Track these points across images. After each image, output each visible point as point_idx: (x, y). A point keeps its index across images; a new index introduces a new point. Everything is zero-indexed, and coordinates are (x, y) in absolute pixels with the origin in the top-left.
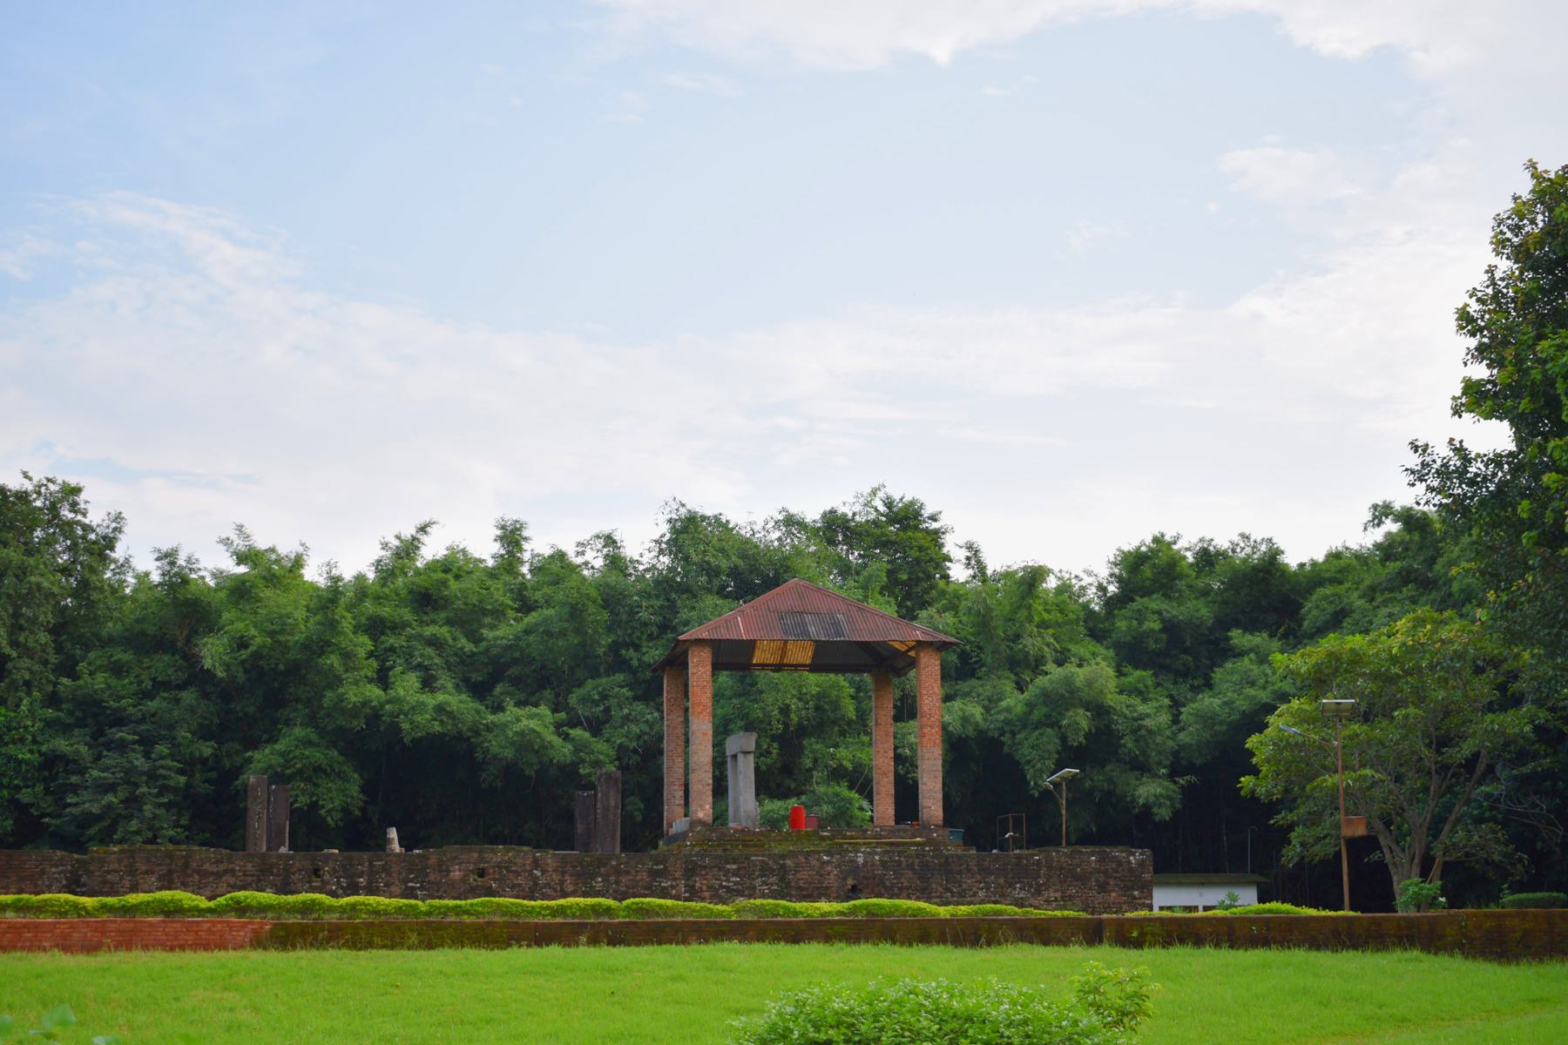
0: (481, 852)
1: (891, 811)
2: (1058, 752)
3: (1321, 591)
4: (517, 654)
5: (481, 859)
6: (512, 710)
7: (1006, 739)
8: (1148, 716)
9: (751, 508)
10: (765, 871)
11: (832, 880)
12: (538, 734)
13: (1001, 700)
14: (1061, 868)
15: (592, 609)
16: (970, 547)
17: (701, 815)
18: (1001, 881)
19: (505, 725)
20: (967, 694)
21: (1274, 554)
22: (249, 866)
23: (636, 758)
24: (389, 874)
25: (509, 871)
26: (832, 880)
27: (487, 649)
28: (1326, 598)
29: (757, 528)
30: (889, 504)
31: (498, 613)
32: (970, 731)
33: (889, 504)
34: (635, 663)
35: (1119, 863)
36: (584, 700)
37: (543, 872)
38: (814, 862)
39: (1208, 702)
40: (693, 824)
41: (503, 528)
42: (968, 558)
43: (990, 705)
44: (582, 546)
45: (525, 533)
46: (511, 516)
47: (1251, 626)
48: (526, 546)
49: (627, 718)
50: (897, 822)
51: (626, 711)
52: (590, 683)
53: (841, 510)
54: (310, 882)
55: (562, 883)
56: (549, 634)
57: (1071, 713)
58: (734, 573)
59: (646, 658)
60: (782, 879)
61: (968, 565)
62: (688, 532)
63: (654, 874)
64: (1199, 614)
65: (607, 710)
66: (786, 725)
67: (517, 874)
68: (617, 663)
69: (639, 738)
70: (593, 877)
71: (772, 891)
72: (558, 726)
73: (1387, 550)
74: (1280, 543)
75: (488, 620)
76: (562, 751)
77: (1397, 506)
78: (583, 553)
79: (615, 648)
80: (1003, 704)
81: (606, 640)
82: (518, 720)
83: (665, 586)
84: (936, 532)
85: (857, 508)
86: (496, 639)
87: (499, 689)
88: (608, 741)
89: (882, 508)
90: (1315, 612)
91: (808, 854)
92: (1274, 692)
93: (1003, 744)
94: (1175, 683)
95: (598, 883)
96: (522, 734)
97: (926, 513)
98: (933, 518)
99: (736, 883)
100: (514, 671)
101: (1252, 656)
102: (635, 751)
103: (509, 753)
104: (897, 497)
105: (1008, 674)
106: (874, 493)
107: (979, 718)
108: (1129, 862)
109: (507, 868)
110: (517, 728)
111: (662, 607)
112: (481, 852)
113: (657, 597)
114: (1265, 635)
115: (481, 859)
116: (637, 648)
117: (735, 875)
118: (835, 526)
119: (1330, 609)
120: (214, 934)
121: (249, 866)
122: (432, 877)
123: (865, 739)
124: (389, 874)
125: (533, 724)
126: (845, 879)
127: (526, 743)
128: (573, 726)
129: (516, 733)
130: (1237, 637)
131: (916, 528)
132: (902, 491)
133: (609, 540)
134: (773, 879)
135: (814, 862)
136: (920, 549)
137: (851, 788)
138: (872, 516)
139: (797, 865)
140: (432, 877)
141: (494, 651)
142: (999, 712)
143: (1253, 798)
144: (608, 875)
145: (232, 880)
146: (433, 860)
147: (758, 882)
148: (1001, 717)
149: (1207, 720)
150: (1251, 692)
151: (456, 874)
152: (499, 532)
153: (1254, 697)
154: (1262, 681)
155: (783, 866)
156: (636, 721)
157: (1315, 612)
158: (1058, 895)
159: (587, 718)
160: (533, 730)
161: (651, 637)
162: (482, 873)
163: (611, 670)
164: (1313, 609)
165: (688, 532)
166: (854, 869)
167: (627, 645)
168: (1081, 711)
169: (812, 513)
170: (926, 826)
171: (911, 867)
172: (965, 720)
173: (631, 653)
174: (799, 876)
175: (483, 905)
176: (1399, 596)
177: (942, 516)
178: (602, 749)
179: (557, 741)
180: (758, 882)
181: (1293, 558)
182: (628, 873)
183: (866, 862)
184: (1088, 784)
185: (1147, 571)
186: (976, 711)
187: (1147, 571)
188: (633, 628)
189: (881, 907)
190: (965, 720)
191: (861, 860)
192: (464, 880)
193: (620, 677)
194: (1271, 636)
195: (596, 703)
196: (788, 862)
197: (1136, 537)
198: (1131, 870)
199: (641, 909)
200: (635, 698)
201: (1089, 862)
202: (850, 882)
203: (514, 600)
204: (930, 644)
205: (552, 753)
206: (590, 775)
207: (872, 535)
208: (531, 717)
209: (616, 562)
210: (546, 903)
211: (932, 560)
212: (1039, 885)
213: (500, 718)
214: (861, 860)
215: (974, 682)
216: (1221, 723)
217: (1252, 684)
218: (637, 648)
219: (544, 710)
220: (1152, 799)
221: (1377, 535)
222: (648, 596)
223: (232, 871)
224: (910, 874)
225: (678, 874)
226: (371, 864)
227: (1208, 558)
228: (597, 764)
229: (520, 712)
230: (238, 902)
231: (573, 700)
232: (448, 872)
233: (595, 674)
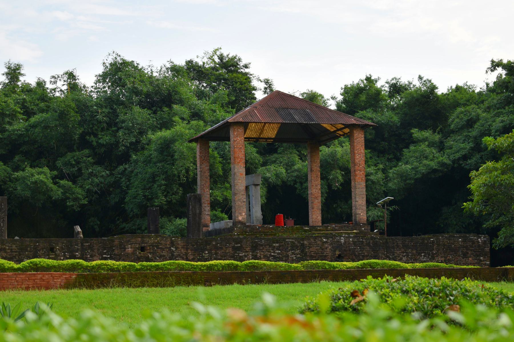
0: (143, 237)
1: (320, 218)
2: (327, 193)
3: (459, 110)
4: (27, 139)
5: (143, 242)
6: (29, 170)
7: (298, 186)
8: (372, 174)
9: (154, 59)
10: (294, 247)
11: (328, 251)
12: (45, 183)
13: (293, 165)
14: (444, 245)
15: (72, 113)
16: (267, 82)
17: (240, 218)
18: (414, 252)
19: (24, 178)
20: (274, 162)
21: (433, 88)
22: (14, 247)
23: (96, 196)
24: (93, 250)
25: (158, 248)
26: (328, 251)
27: (9, 136)
28: (462, 113)
29: (154, 69)
30: (221, 57)
31: (13, 116)
32: (279, 183)
33: (221, 57)
34: (95, 143)
35: (473, 243)
36: (66, 164)
37: (177, 248)
38: (319, 242)
39: (404, 167)
40: (235, 224)
41: (9, 68)
42: (266, 88)
43: (289, 166)
44: (55, 79)
45: (22, 72)
46: (14, 61)
47: (422, 127)
48: (21, 78)
49: (91, 174)
50: (323, 223)
51: (90, 170)
52: (69, 155)
53: (195, 60)
54: (48, 255)
55: (186, 254)
56: (46, 127)
57: (333, 172)
58: (148, 95)
59: (101, 141)
60: (302, 251)
61: (265, 92)
62: (119, 72)
63: (235, 249)
64: (393, 120)
65: (80, 170)
66: (187, 180)
67: (163, 250)
68: (84, 143)
69: (98, 185)
70: (203, 251)
71: (297, 258)
72: (53, 178)
73: (500, 85)
74: (435, 82)
75: (7, 119)
76: (57, 193)
77: (505, 61)
78: (55, 83)
79: (83, 136)
80: (296, 167)
81: (80, 131)
82: (33, 175)
83: (110, 102)
84: (246, 74)
85: (205, 60)
86: (14, 130)
87: (17, 158)
88: (81, 187)
89: (217, 60)
90: (457, 120)
91: (315, 238)
92: (439, 163)
93: (296, 188)
94: (378, 157)
95: (206, 254)
96: (36, 183)
97: (242, 64)
98: (246, 66)
99: (278, 254)
100: (24, 148)
101: (427, 143)
102: (96, 192)
103: (28, 193)
104: (225, 54)
105: (295, 151)
106: (215, 52)
107: (285, 174)
108: (478, 242)
109: (156, 246)
110: (33, 179)
111: (109, 113)
112: (143, 237)
113: (106, 107)
114: (431, 132)
115: (143, 242)
116: (96, 135)
117: (278, 249)
118: (193, 70)
119: (466, 118)
120: (44, 280)
121: (14, 247)
122: (116, 252)
123: (227, 185)
124: (93, 250)
125: (42, 177)
126: (335, 251)
127: (37, 188)
128: (62, 179)
129: (32, 183)
130: (416, 133)
131: (237, 72)
132: (229, 51)
133: (71, 76)
134: (298, 251)
135: (319, 242)
136: (241, 83)
137: (222, 212)
138: (212, 65)
139: (310, 244)
140: (116, 252)
141: (13, 137)
142: (293, 172)
143: (471, 215)
144: (211, 250)
145: (4, 255)
146: (116, 242)
147: (290, 253)
148: (295, 174)
149: (403, 176)
150: (425, 162)
151: (129, 250)
152: (6, 70)
153: (429, 165)
154: (431, 156)
155: (303, 245)
156: (96, 176)
157: (457, 120)
158: (443, 259)
159: (68, 174)
160: (42, 181)
161: (103, 130)
162: (143, 249)
163: (80, 148)
164: (455, 118)
165: (119, 72)
166: (339, 246)
167: (89, 134)
168: (339, 171)
169: (181, 62)
170: (357, 225)
171: (368, 244)
172: (277, 175)
173: (92, 138)
174: (311, 249)
175: (170, 264)
176: (504, 111)
177: (251, 66)
178: (79, 192)
179: (55, 187)
180: (290, 253)
181: (442, 90)
182: (222, 248)
183: (345, 242)
184: (339, 210)
185: (363, 98)
186: (282, 170)
187: (363, 98)
188: (93, 124)
189: (378, 264)
190: (277, 175)
191: (343, 241)
192: (134, 253)
193: (86, 151)
194: (434, 132)
195: (73, 166)
196: (305, 242)
197: (355, 78)
198: (479, 246)
199: (254, 266)
200: (94, 163)
201: (458, 242)
202: (337, 253)
203: (21, 109)
204: (359, 126)
205: (52, 193)
206: (73, 206)
207: (214, 75)
208: (39, 173)
209: (73, 86)
210: (203, 263)
211: (247, 90)
212: (433, 254)
213: (20, 174)
214: (343, 241)
215: (276, 155)
216: (410, 179)
217: (426, 158)
218: (96, 135)
219: (46, 169)
220: (376, 218)
221: (492, 78)
222: (101, 107)
223: (5, 249)
224: (368, 248)
225: (248, 249)
226: (82, 245)
227: (396, 89)
228: (76, 199)
229: (33, 171)
230: (36, 265)
231: (59, 163)
232: (125, 249)
233: (71, 149)
